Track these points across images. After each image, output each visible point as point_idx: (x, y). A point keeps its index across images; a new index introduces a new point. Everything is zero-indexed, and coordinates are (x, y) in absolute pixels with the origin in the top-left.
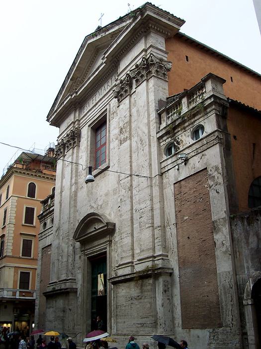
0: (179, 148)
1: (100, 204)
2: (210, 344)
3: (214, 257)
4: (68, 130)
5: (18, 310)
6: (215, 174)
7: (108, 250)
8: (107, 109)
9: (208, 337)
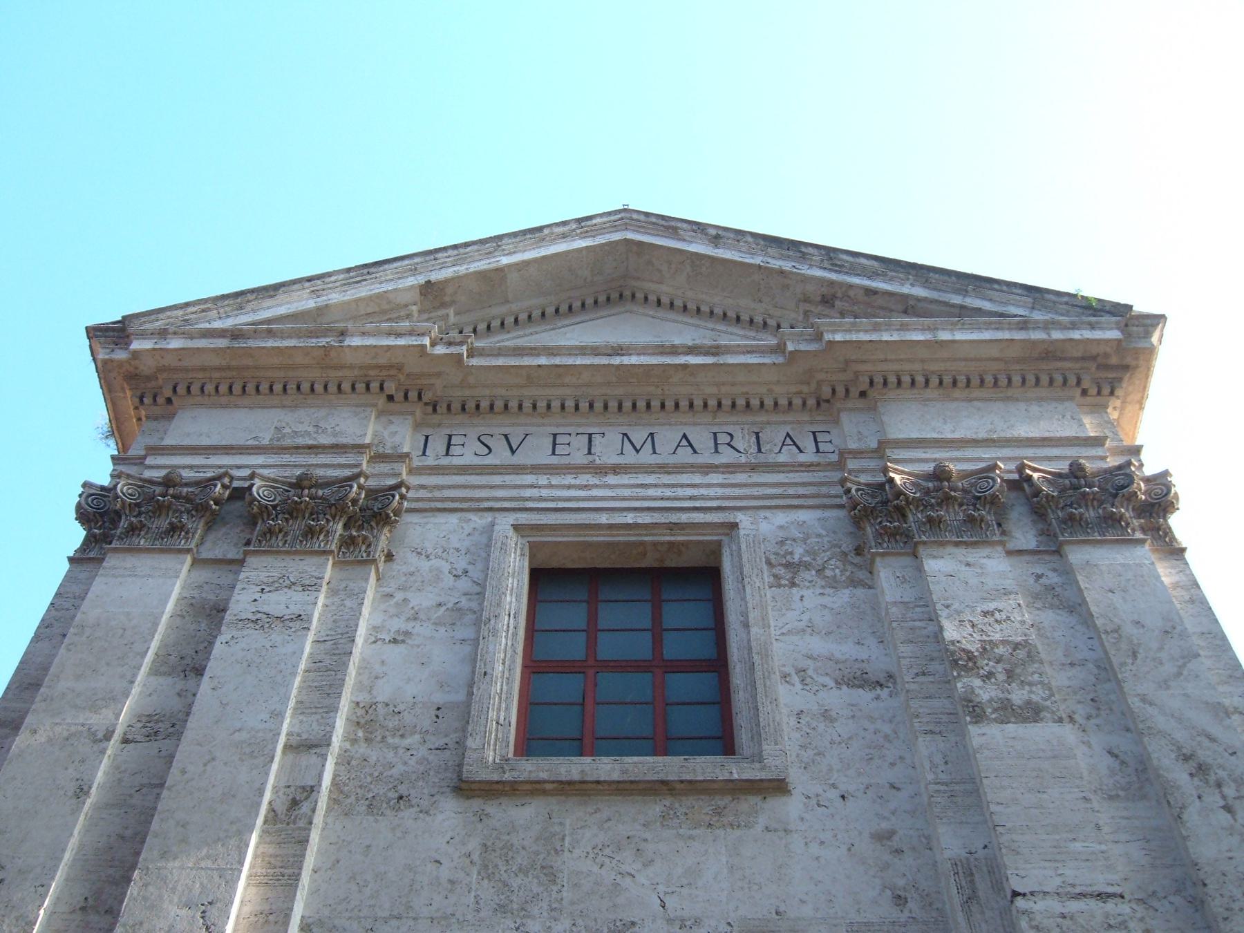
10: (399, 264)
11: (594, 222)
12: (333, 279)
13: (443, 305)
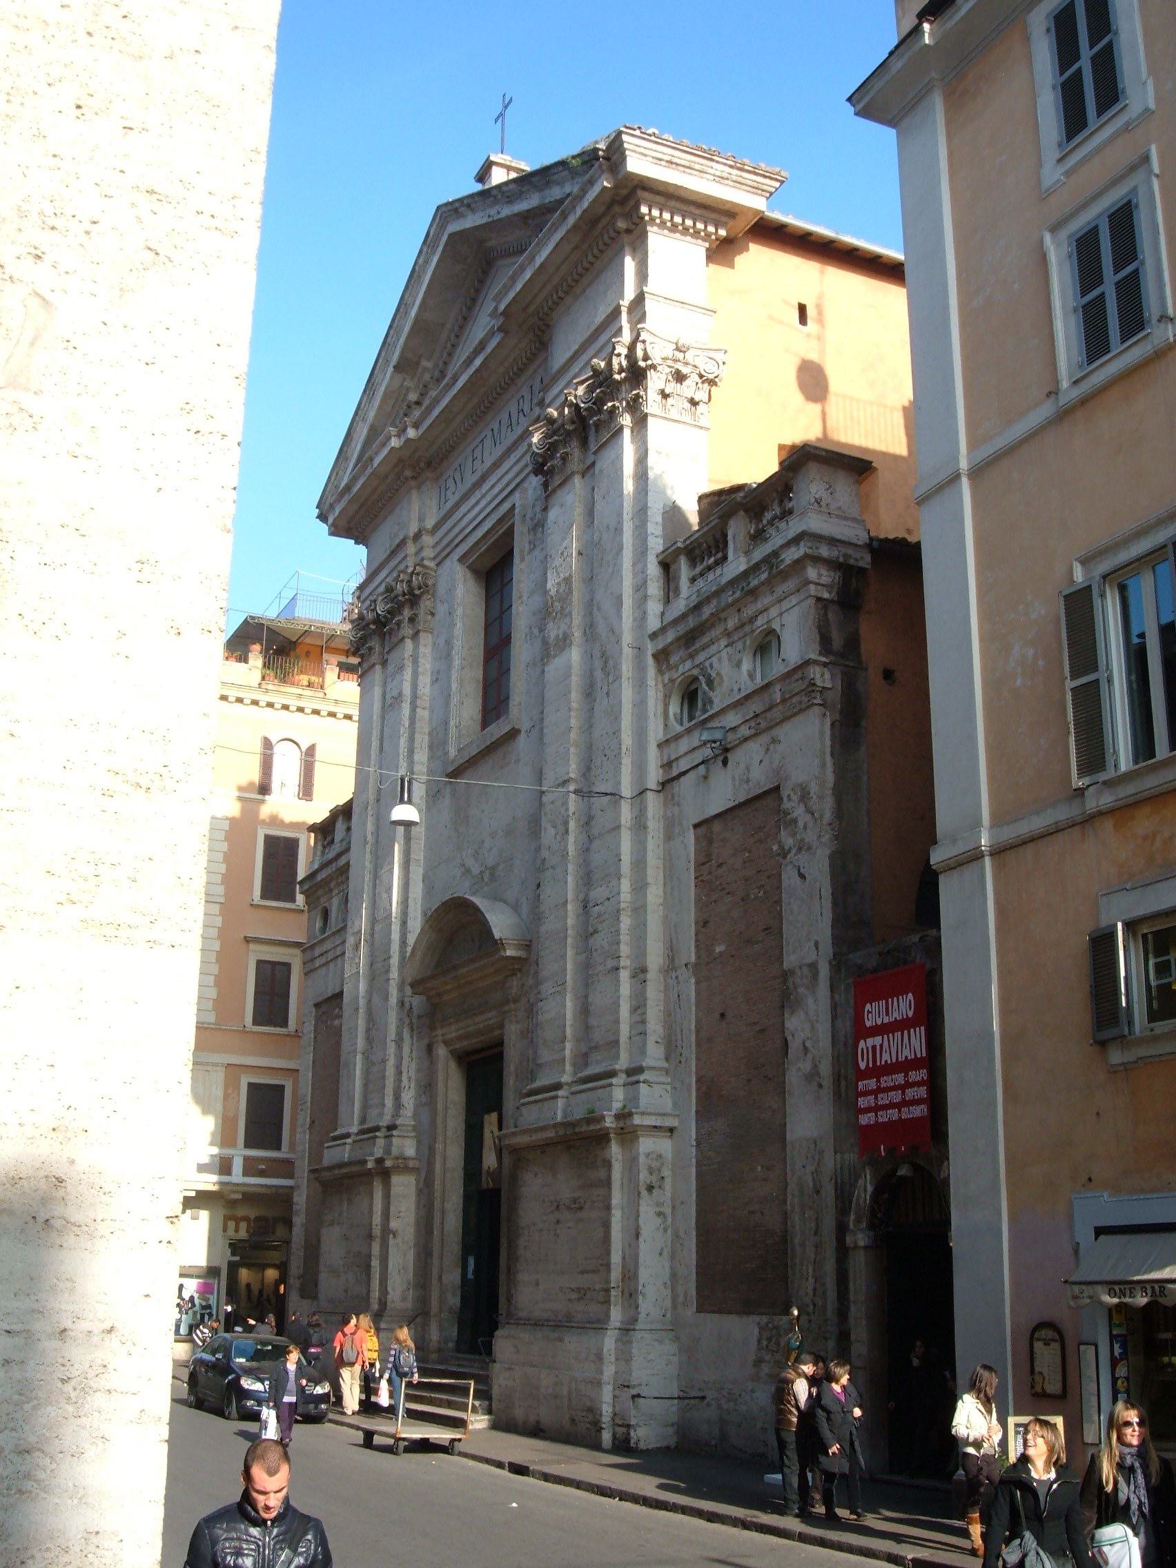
0: (711, 702)
1: (490, 861)
2: (758, 1362)
3: (781, 1090)
4: (392, 564)
5: (243, 1225)
6: (799, 812)
7: (512, 1032)
8: (513, 507)
9: (755, 1339)
10: (379, 364)
11: (431, 234)
12: (363, 405)
13: (418, 363)
